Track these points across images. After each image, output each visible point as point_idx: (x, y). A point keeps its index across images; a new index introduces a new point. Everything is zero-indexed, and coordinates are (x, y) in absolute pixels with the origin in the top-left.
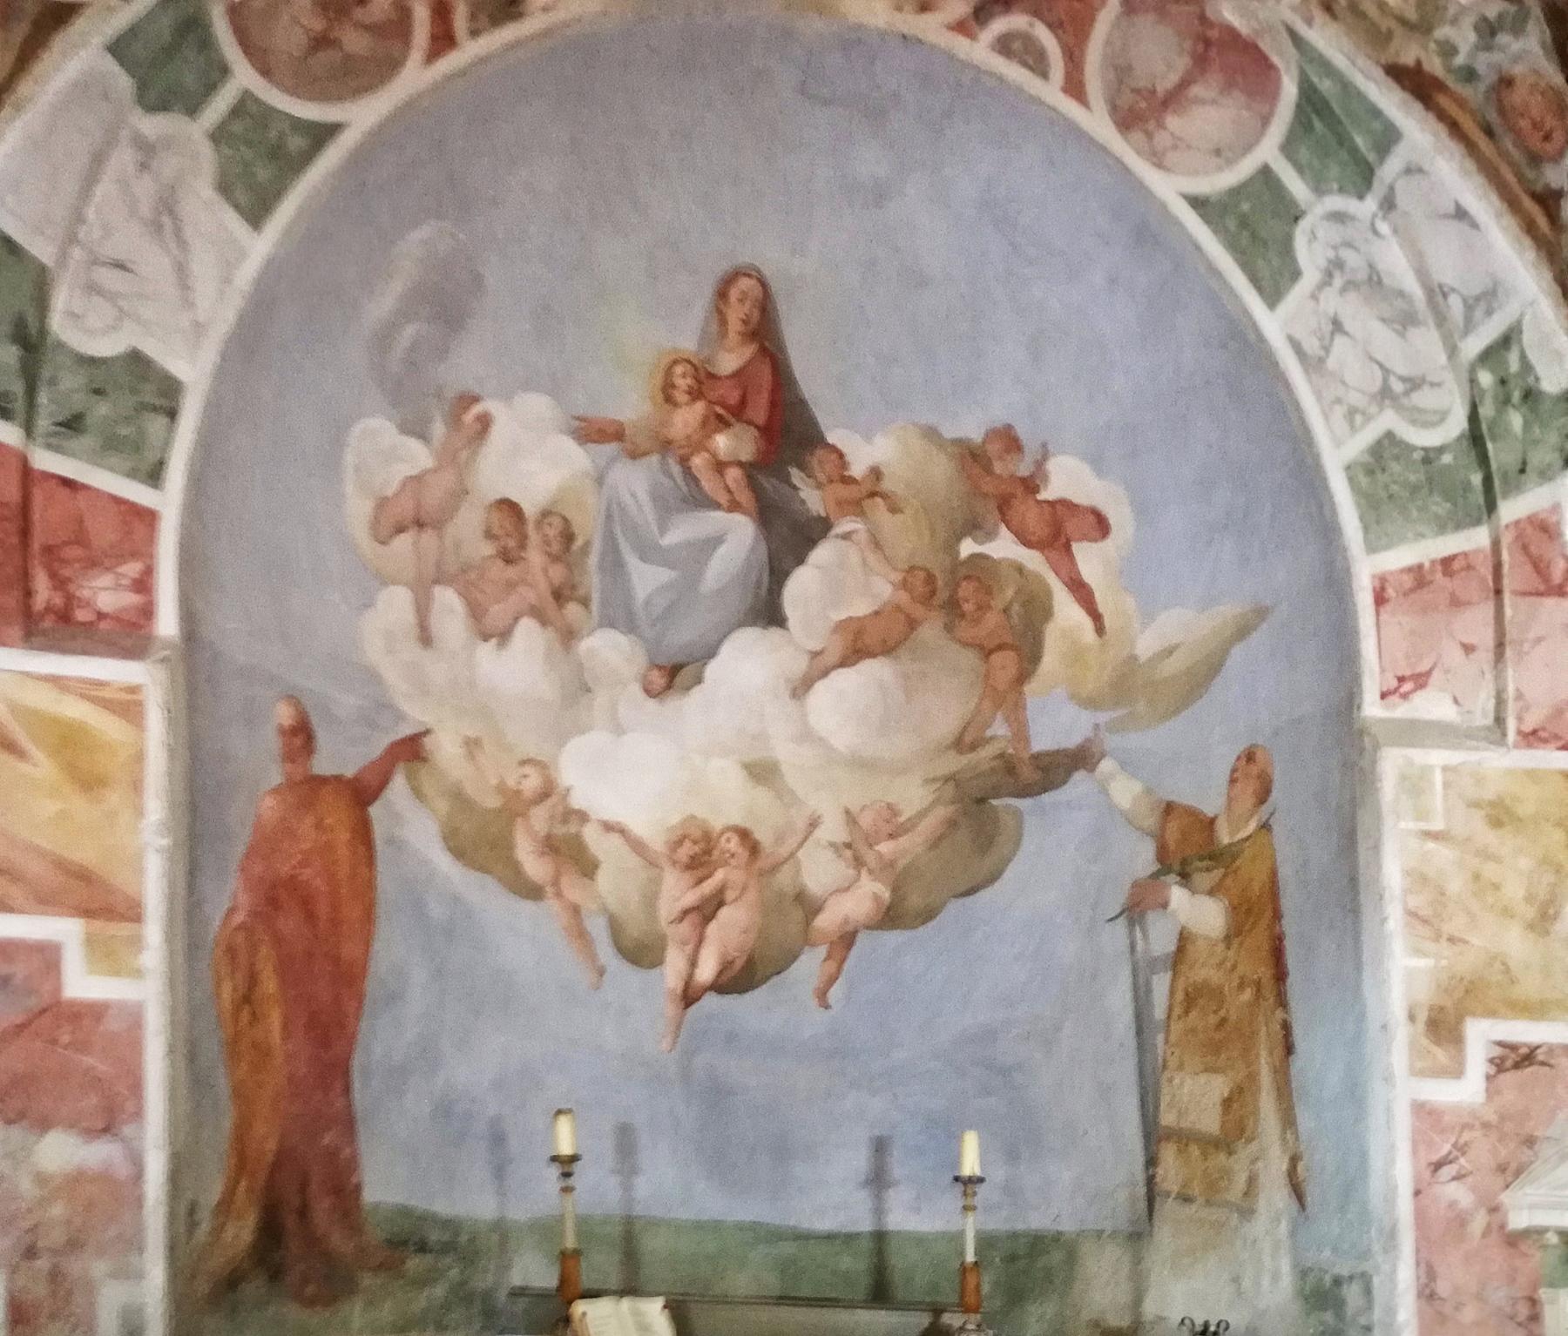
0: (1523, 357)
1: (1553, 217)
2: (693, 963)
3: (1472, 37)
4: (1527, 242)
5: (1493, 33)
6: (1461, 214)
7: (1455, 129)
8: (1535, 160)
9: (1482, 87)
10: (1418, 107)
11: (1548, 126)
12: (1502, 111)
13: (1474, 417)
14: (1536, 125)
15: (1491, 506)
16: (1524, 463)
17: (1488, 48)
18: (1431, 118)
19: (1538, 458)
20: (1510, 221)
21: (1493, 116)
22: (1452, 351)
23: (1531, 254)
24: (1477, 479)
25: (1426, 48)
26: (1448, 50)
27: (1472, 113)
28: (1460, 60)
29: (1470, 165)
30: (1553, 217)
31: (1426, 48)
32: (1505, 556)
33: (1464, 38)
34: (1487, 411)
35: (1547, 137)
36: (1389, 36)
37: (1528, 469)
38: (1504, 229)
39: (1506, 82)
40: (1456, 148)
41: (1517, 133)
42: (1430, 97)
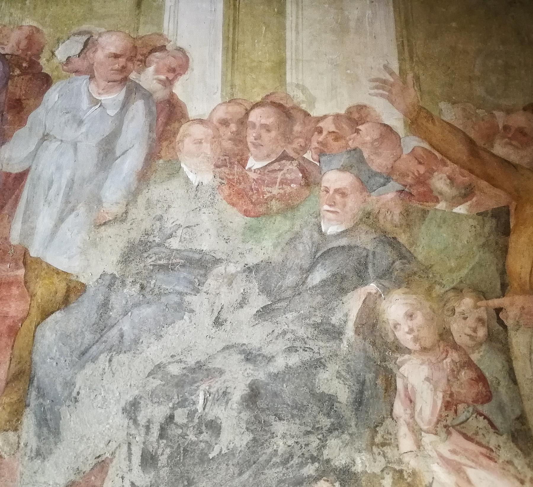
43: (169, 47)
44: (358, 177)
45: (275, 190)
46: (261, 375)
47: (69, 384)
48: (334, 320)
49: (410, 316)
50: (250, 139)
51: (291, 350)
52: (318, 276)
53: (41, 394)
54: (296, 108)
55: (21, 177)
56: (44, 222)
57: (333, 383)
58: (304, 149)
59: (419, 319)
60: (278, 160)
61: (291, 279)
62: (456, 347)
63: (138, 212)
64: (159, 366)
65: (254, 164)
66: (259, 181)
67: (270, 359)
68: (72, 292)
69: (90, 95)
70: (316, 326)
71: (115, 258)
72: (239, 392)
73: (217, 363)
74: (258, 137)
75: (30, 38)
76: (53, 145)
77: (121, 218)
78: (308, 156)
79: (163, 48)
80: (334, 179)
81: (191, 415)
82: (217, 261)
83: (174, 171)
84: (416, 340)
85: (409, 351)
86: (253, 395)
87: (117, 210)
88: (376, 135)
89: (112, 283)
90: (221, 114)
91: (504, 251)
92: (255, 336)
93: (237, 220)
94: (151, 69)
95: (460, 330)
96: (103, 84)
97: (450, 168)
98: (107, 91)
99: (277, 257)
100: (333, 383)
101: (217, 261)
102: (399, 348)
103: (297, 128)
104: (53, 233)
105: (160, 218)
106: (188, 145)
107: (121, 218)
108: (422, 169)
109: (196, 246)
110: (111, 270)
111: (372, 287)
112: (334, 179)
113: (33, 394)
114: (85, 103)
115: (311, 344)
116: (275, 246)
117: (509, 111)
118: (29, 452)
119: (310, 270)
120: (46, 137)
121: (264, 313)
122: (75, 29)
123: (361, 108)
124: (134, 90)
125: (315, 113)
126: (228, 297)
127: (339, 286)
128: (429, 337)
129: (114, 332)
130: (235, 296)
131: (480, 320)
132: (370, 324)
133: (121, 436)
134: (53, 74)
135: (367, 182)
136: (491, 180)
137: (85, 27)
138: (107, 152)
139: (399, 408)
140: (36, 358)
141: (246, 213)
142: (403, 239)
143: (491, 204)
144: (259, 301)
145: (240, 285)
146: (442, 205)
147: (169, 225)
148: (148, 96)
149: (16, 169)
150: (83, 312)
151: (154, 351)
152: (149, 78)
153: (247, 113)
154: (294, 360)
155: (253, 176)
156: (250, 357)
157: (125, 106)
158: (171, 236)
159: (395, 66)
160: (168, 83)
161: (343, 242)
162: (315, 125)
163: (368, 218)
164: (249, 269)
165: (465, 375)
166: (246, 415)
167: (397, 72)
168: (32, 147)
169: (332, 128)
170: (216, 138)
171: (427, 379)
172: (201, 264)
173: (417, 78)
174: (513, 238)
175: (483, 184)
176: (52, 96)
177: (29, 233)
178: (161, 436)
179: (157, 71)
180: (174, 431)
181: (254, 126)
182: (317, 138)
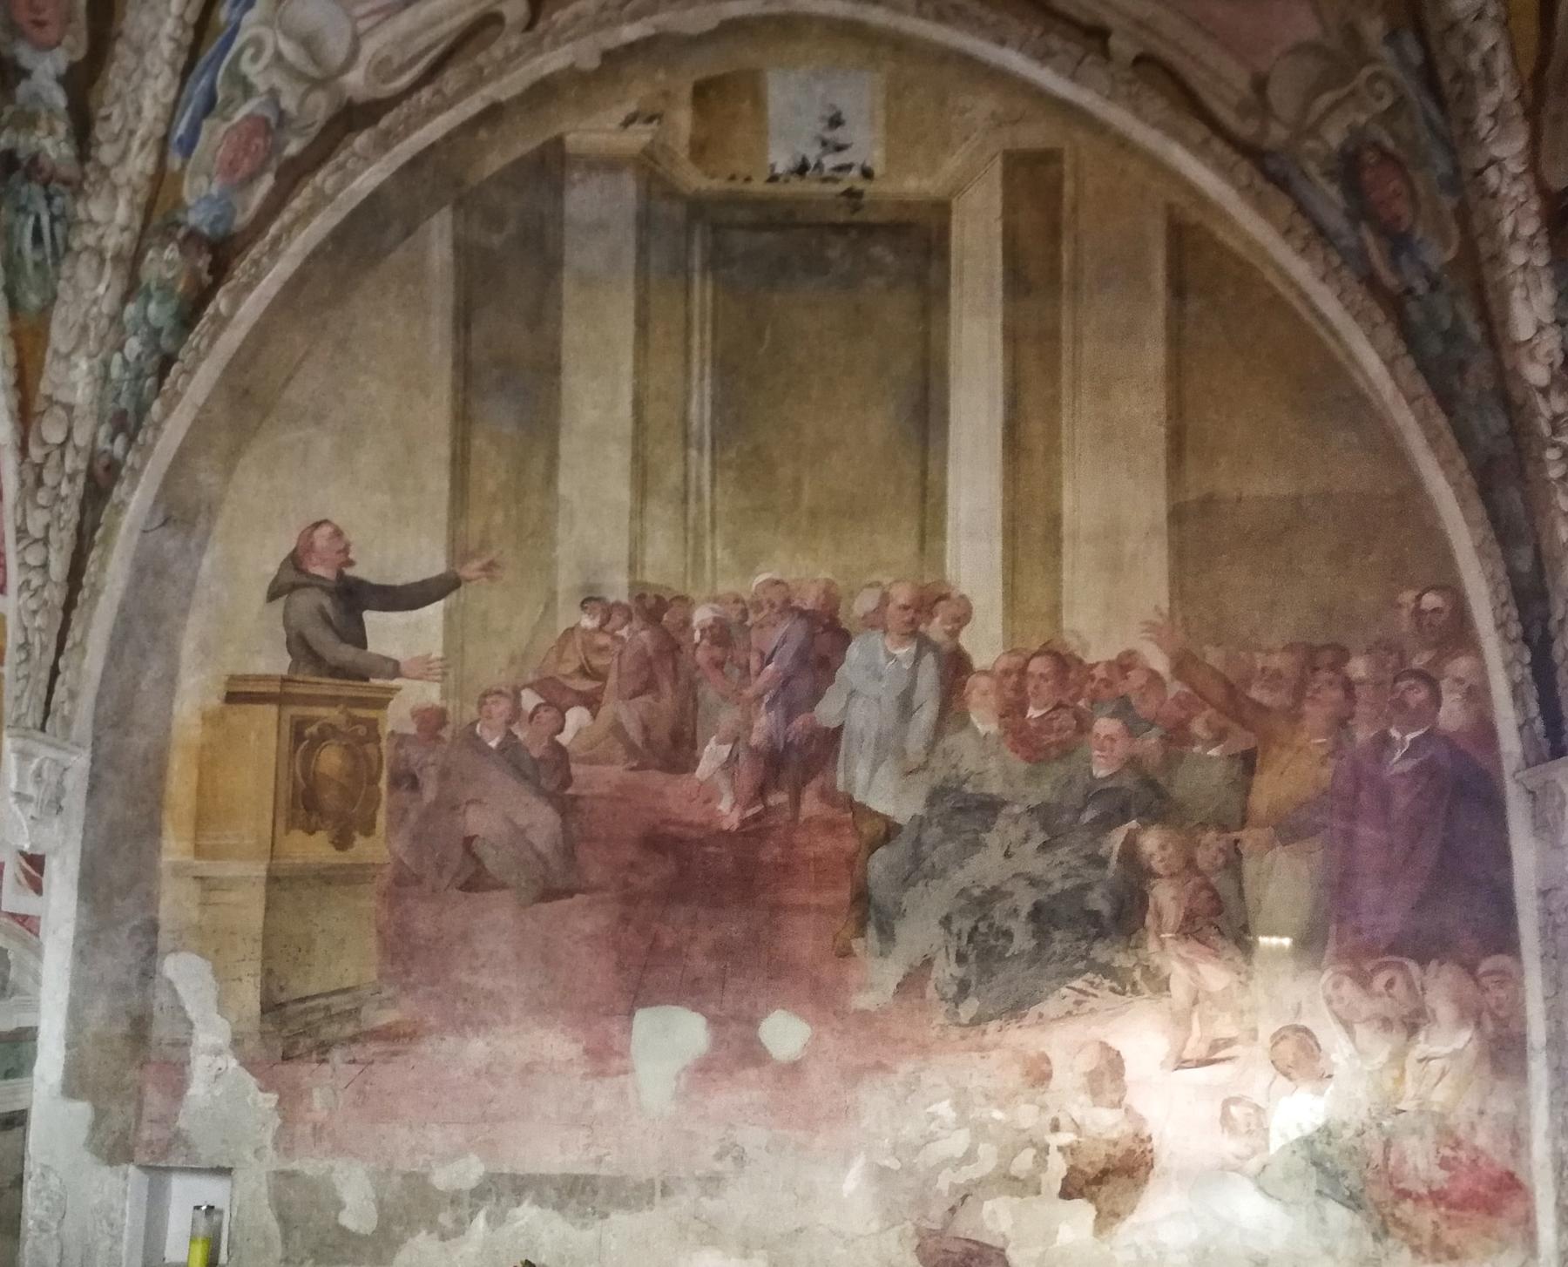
43: (954, 595)
44: (1125, 723)
45: (1053, 738)
46: (1042, 897)
47: (898, 904)
48: (1101, 852)
49: (1163, 847)
50: (1030, 689)
51: (1065, 877)
52: (1088, 816)
53: (878, 910)
54: (1071, 655)
55: (840, 728)
56: (861, 772)
57: (1098, 901)
58: (1077, 697)
59: (1170, 849)
60: (1055, 709)
61: (1067, 817)
62: (1199, 873)
63: (936, 762)
64: (963, 890)
65: (1033, 713)
66: (1039, 729)
67: (1049, 884)
68: (890, 832)
69: (886, 650)
70: (1086, 857)
71: (922, 802)
72: (1026, 908)
73: (1009, 887)
74: (1036, 687)
75: (826, 592)
76: (860, 702)
77: (923, 767)
78: (1081, 703)
79: (945, 597)
80: (1105, 726)
81: (991, 926)
82: (1004, 803)
83: (965, 722)
84: (1167, 867)
85: (1161, 877)
86: (1037, 912)
87: (921, 759)
88: (1143, 681)
89: (920, 823)
90: (1001, 666)
91: (1247, 791)
92: (1037, 866)
93: (1021, 766)
94: (937, 620)
95: (1203, 858)
96: (897, 638)
97: (1209, 712)
98: (901, 644)
99: (1054, 799)
100: (1098, 901)
101: (1004, 803)
102: (1151, 874)
103: (1072, 675)
104: (870, 783)
105: (955, 766)
106: (974, 697)
107: (923, 767)
108: (1183, 715)
109: (986, 790)
110: (919, 812)
111: (1133, 824)
112: (1105, 726)
113: (872, 912)
114: (882, 659)
115: (1082, 871)
116: (1053, 789)
117: (1270, 652)
118: (413, 817)
119: (1081, 811)
120: (852, 693)
121: (1045, 847)
122: (868, 580)
123: (1130, 654)
124: (924, 643)
125: (1089, 660)
126: (1015, 834)
127: (1106, 823)
128: (1177, 864)
129: (927, 864)
130: (1020, 833)
131: (1221, 850)
132: (1130, 852)
133: (940, 941)
134: (852, 630)
135: (1134, 726)
136: (1243, 723)
137: (876, 577)
138: (906, 706)
139: (1149, 919)
140: (870, 884)
141: (1028, 759)
142: (1162, 780)
143: (1241, 747)
144: (1039, 837)
145: (1025, 820)
146: (1197, 749)
147: (963, 772)
148: (936, 648)
149: (834, 724)
150: (901, 847)
151: (960, 878)
152: (936, 630)
153: (1028, 662)
154: (1068, 884)
155: (1033, 724)
156: (1033, 882)
157: (917, 658)
158: (965, 781)
159: (1165, 606)
160: (954, 634)
161: (1110, 784)
162: (1087, 671)
163: (1133, 762)
164: (1031, 810)
165: (1204, 894)
166: (1030, 927)
167: (1166, 612)
168: (843, 705)
169: (1104, 675)
170: (1000, 686)
171: (1174, 898)
172: (990, 807)
173: (1185, 619)
174: (1257, 778)
175: (1236, 727)
176: (854, 652)
177: (849, 783)
178: (969, 941)
179: (943, 622)
180: (979, 938)
181: (1032, 675)
182: (1090, 686)
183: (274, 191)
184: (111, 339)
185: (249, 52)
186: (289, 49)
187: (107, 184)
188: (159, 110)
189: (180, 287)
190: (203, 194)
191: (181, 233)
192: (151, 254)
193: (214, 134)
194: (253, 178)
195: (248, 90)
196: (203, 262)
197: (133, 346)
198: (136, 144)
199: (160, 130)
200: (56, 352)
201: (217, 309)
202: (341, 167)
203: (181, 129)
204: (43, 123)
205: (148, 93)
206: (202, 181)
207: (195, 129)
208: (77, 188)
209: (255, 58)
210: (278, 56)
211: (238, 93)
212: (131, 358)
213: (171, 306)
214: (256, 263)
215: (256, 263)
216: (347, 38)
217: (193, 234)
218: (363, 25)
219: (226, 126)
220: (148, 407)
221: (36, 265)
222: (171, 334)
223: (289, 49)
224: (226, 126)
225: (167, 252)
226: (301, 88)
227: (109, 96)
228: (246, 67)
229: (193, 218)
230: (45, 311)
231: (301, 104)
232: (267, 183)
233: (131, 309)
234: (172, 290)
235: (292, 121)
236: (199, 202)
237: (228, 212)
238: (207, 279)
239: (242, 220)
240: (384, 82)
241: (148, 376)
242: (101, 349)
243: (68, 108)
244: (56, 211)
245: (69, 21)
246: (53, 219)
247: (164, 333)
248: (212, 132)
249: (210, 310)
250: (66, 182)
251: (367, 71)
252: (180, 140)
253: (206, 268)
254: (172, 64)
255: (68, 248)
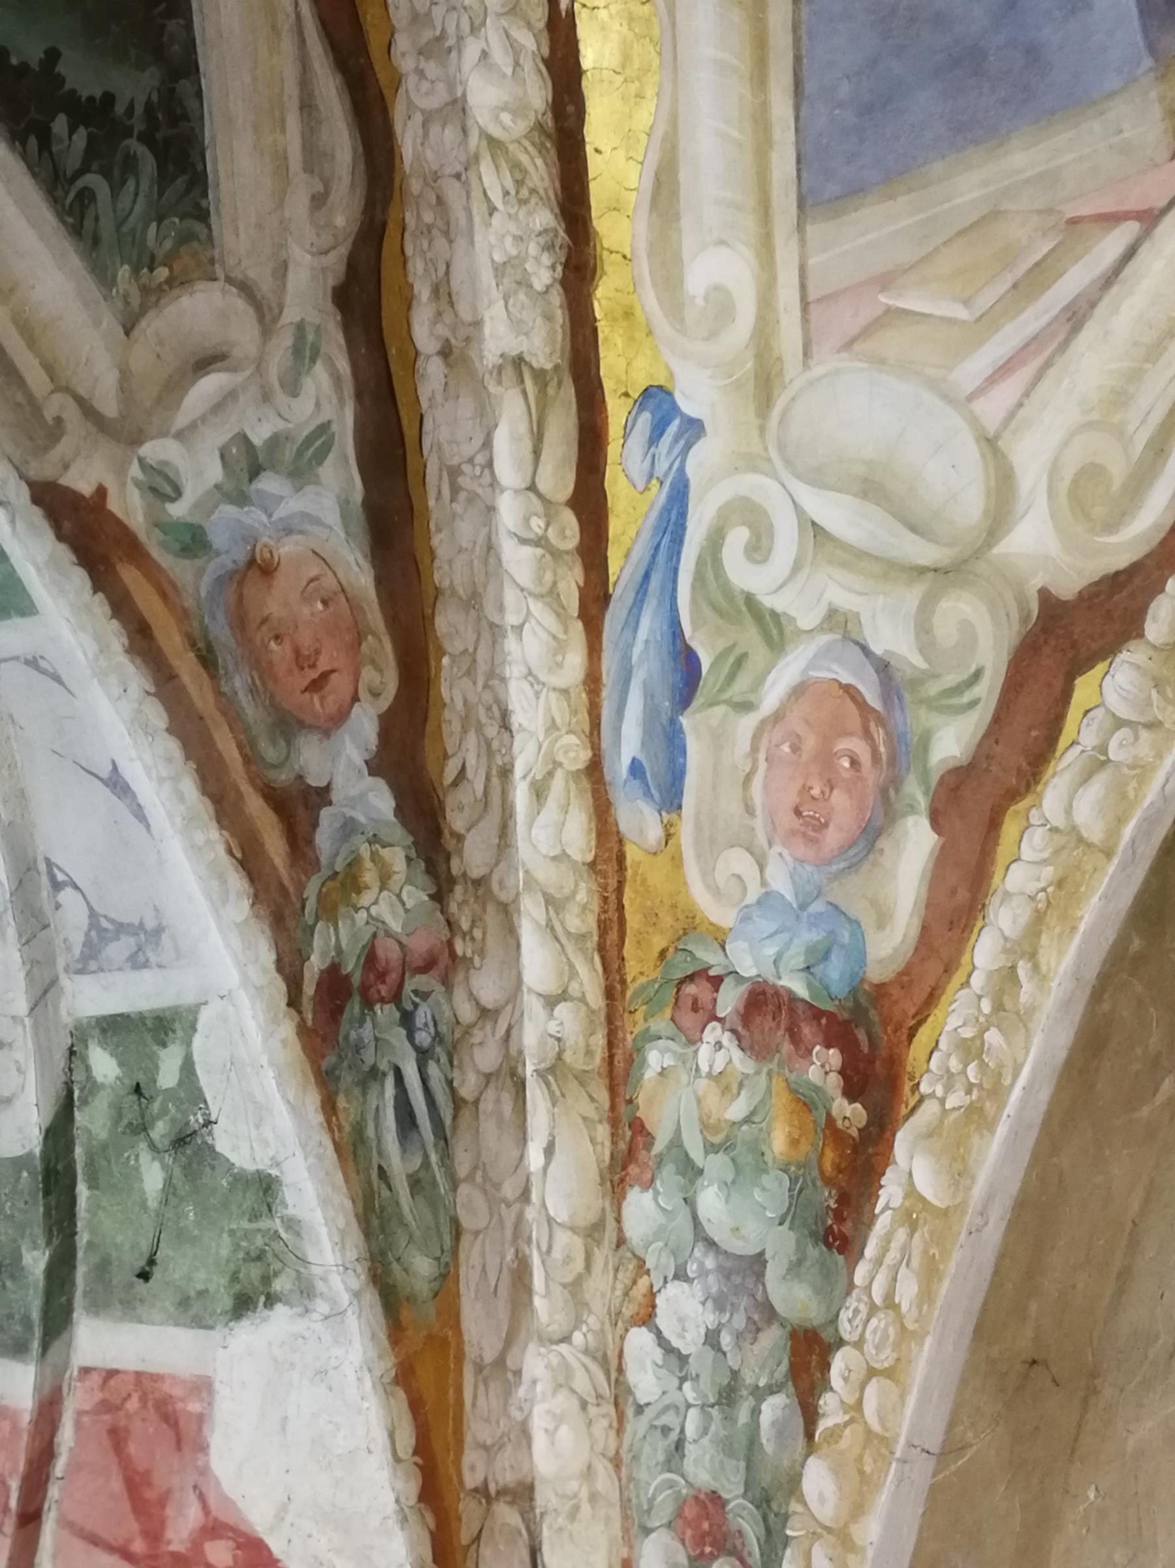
0: (188, 1067)
1: (299, 841)
2: (1129, 254)
3: (215, 472)
4: (237, 882)
5: (255, 472)
6: (117, 783)
7: (142, 640)
8: (288, 725)
9: (214, 567)
10: (79, 578)
11: (323, 665)
12: (240, 622)
13: (60, 1132)
14: (301, 660)
15: (56, 1322)
16: (152, 1262)
17: (241, 499)
18: (99, 605)
19: (177, 1266)
20: (213, 837)
21: (221, 632)
22: (44, 993)
23: (240, 907)
24: (36, 1261)
25: (121, 471)
26: (162, 486)
27: (183, 616)
28: (177, 510)
29: (157, 716)
30: (299, 841)
31: (121, 471)
32: (66, 1436)
33: (200, 470)
34: (93, 1122)
35: (317, 685)
36: (56, 430)
37: (157, 1273)
38: (194, 850)
39: (260, 568)
40: (136, 679)
41: (261, 666)
42: (110, 568)
183: (942, 861)
184: (602, 1287)
185: (737, 538)
186: (836, 513)
187: (491, 908)
188: (559, 710)
189: (778, 1143)
190: (752, 897)
191: (729, 1000)
192: (655, 1059)
193: (716, 742)
194: (872, 834)
195: (774, 630)
196: (822, 1068)
197: (685, 1310)
198: (521, 796)
199: (577, 755)
200: (479, 1368)
201: (911, 1191)
202: (1099, 762)
203: (629, 742)
204: (369, 876)
205: (513, 672)
206: (739, 862)
207: (672, 742)
208: (444, 964)
209: (758, 550)
210: (816, 533)
211: (750, 637)
212: (690, 1343)
213: (772, 1193)
214: (971, 1050)
215: (971, 1050)
216: (970, 451)
217: (762, 1001)
218: (992, 409)
219: (747, 724)
220: (793, 1484)
221: (415, 1183)
222: (795, 1268)
223: (836, 513)
224: (747, 724)
225: (704, 1051)
226: (912, 596)
227: (452, 726)
228: (741, 574)
229: (748, 960)
230: (447, 1279)
231: (923, 627)
232: (916, 844)
233: (642, 1210)
234: (758, 1152)
235: (916, 683)
236: (745, 918)
237: (841, 929)
238: (851, 1114)
239: (889, 944)
240: (1111, 527)
241: (760, 1394)
242: (578, 1323)
243: (399, 811)
244: (423, 1038)
245: (360, 638)
246: (423, 1056)
247: (773, 1272)
248: (718, 739)
249: (890, 1192)
250: (427, 966)
251: (1054, 515)
252: (636, 768)
253: (834, 1082)
254: (551, 596)
255: (458, 1102)
